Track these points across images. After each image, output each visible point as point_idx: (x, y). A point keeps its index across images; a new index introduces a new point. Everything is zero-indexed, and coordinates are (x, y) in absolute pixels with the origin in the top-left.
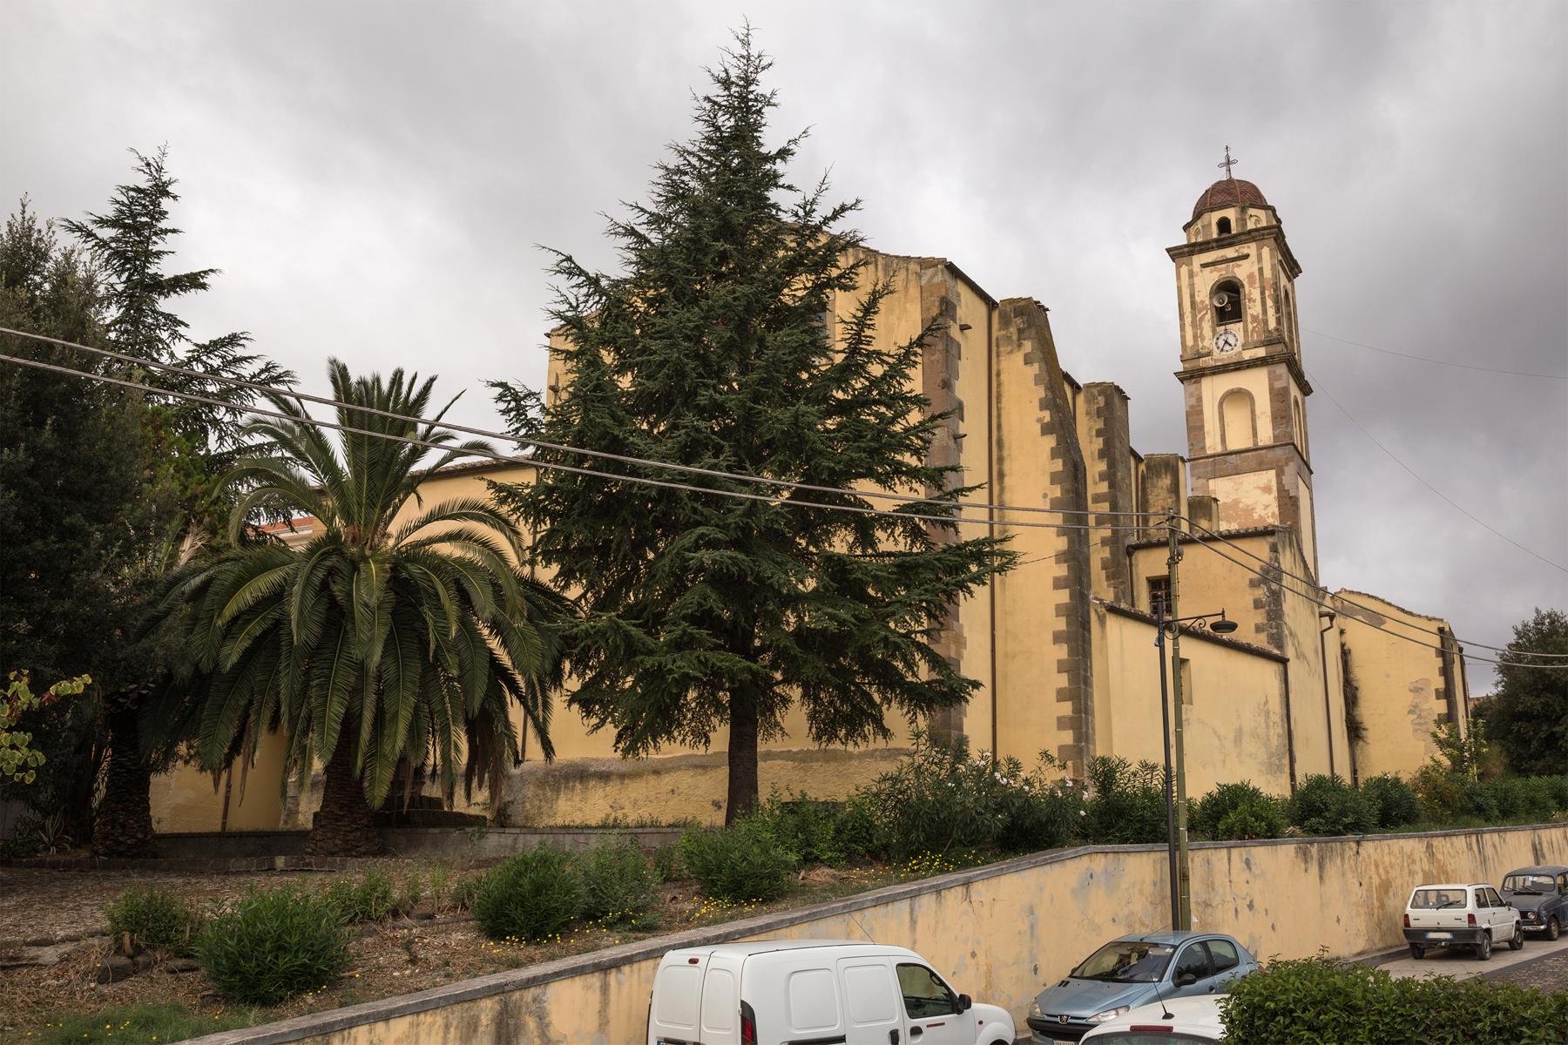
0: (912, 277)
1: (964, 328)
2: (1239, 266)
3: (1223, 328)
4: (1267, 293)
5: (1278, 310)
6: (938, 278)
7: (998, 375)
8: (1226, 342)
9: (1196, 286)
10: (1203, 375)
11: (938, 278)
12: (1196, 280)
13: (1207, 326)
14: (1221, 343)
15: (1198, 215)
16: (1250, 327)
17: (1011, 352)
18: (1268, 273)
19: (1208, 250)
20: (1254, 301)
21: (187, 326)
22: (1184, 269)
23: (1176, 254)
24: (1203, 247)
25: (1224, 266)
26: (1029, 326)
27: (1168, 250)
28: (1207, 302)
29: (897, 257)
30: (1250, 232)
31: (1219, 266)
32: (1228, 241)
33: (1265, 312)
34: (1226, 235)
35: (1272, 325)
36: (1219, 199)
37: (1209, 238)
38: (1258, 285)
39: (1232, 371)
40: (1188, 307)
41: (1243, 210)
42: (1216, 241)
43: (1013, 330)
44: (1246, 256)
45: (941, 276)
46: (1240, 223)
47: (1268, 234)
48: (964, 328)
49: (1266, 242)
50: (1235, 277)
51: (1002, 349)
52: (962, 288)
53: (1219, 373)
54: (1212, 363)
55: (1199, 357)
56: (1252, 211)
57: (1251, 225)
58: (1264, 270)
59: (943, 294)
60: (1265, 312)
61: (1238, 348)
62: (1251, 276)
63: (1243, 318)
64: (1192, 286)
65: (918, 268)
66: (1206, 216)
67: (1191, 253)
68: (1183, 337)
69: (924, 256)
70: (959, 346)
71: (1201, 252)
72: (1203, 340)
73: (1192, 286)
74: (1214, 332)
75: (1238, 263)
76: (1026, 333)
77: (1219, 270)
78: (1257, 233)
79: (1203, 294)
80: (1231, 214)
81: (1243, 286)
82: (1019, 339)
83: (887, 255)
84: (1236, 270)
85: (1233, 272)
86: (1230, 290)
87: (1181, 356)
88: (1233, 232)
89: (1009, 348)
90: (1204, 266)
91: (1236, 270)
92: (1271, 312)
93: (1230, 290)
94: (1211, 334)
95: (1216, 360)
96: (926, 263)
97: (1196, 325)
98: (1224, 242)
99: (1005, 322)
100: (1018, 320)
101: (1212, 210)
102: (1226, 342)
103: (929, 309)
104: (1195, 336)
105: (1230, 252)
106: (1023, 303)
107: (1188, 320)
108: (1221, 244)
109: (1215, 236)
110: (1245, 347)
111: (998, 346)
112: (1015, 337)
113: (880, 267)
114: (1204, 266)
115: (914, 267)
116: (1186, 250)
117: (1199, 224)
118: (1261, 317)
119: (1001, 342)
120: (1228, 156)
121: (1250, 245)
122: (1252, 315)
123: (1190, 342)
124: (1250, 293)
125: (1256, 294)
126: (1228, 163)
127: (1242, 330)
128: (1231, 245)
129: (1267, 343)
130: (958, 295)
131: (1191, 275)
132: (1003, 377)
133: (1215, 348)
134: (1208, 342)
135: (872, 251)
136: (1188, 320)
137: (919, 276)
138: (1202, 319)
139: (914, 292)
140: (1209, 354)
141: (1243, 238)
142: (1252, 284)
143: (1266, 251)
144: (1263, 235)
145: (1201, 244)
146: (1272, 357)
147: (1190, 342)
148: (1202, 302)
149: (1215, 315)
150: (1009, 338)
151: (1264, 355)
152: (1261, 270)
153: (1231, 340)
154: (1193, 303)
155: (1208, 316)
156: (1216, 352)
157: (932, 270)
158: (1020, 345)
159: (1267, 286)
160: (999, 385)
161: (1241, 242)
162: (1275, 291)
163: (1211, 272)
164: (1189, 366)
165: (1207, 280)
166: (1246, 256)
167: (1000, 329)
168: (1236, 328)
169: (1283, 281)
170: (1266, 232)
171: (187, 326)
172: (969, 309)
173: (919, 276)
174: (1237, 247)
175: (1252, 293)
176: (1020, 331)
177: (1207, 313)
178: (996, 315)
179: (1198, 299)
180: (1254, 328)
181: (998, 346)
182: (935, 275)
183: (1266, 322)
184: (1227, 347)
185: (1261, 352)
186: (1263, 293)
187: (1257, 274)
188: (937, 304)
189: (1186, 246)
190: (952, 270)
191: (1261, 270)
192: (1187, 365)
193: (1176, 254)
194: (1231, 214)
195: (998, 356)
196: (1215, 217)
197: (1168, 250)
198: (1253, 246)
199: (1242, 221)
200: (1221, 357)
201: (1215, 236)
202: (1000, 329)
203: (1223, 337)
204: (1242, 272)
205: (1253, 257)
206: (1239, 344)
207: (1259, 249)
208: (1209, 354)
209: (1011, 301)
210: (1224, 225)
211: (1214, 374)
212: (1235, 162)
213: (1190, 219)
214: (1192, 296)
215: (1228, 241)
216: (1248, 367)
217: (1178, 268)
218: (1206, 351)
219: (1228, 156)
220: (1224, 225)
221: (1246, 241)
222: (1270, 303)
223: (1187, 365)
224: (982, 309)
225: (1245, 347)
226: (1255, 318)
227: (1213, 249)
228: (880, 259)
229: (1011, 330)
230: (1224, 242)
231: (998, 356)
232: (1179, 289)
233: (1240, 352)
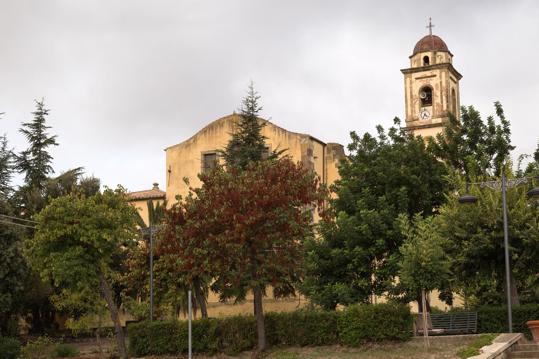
0: (298, 141)
1: (315, 158)
2: (432, 80)
3: (424, 108)
4: (443, 93)
5: (447, 102)
6: (307, 142)
7: (326, 170)
8: (425, 115)
9: (413, 88)
10: (415, 129)
11: (307, 142)
12: (413, 85)
13: (417, 106)
14: (423, 115)
15: (415, 54)
16: (435, 108)
17: (331, 162)
18: (444, 84)
19: (419, 71)
20: (438, 97)
21: (52, 158)
22: (408, 79)
23: (405, 72)
24: (416, 70)
25: (425, 79)
26: (337, 154)
27: (402, 70)
28: (418, 95)
29: (293, 133)
30: (437, 65)
31: (423, 79)
32: (427, 68)
33: (442, 102)
34: (427, 65)
35: (445, 108)
36: (425, 47)
37: (419, 66)
38: (439, 89)
39: (427, 128)
40: (409, 98)
41: (435, 53)
42: (422, 68)
43: (332, 155)
44: (435, 76)
45: (308, 141)
46: (433, 59)
47: (445, 66)
48: (315, 158)
49: (444, 70)
50: (430, 85)
51: (328, 161)
52: (315, 143)
53: (421, 128)
54: (419, 124)
55: (413, 121)
56: (439, 53)
57: (438, 62)
58: (443, 83)
59: (309, 148)
60: (442, 102)
61: (430, 118)
62: (436, 85)
63: (433, 104)
64: (411, 88)
65: (300, 138)
66: (418, 55)
67: (411, 72)
68: (407, 111)
69: (302, 133)
70: (313, 164)
71: (416, 72)
72: (415, 113)
73: (411, 88)
74: (420, 110)
75: (432, 78)
76: (336, 156)
77: (423, 81)
78: (440, 66)
79: (416, 92)
80: (429, 54)
81: (433, 89)
82: (334, 158)
83: (289, 132)
84: (431, 82)
85: (429, 82)
86: (427, 90)
87: (406, 120)
88: (430, 64)
89: (330, 161)
90: (417, 79)
91: (431, 82)
92: (445, 102)
93: (427, 90)
94: (419, 110)
95: (420, 123)
96: (303, 136)
97: (412, 106)
98: (425, 69)
99: (329, 152)
100: (333, 151)
101: (421, 52)
102: (425, 115)
103: (304, 153)
104: (412, 111)
105: (428, 73)
106: (335, 145)
107: (409, 103)
108: (424, 69)
109: (422, 65)
110: (433, 117)
111: (326, 160)
112: (332, 157)
113: (287, 136)
114: (417, 79)
115: (298, 137)
116: (409, 71)
117: (416, 58)
118: (440, 104)
119: (327, 159)
120: (430, 23)
121: (437, 70)
122: (436, 103)
123: (409, 114)
124: (436, 93)
125: (438, 93)
126: (431, 26)
127: (432, 110)
128: (429, 70)
129: (443, 116)
130: (313, 146)
131: (411, 82)
132: (328, 171)
133: (420, 117)
134: (417, 114)
135: (284, 130)
136: (409, 103)
137: (300, 141)
138: (415, 103)
139: (299, 146)
140: (417, 120)
141: (434, 67)
142: (437, 89)
143: (443, 74)
144: (442, 66)
145: (415, 69)
146: (444, 123)
147: (409, 114)
148: (415, 95)
149: (420, 102)
150: (330, 157)
151: (441, 122)
152: (441, 82)
153: (427, 114)
154: (411, 96)
155: (418, 102)
156: (420, 119)
157: (304, 139)
158: (334, 160)
159: (443, 90)
160: (327, 174)
161: (433, 69)
162: (447, 92)
163: (420, 82)
164: (410, 124)
165: (418, 85)
166: (435, 76)
167: (327, 154)
168: (429, 108)
169: (452, 85)
170: (443, 65)
171: (52, 158)
172: (317, 150)
173: (300, 141)
174: (431, 71)
175: (437, 93)
176: (334, 155)
177: (417, 101)
178: (326, 148)
179: (413, 94)
180: (437, 109)
181: (326, 160)
182: (305, 141)
183: (442, 107)
184: (425, 117)
185: (440, 120)
186: (441, 93)
187: (439, 84)
188: (306, 151)
189: (409, 69)
190: (312, 139)
191: (441, 82)
192: (408, 124)
193: (405, 72)
194: (429, 54)
195: (326, 163)
196: (423, 55)
197: (402, 70)
198: (438, 71)
199: (434, 59)
200: (422, 121)
201: (422, 65)
202: (327, 154)
203: (424, 112)
204: (433, 83)
205: (438, 76)
206: (430, 116)
207: (441, 73)
208: (417, 120)
209: (331, 144)
210: (426, 59)
211: (419, 129)
212: (434, 26)
213: (412, 54)
214: (411, 92)
215: (427, 68)
216: (434, 127)
217: (405, 78)
218: (416, 118)
219: (430, 23)
220: (426, 59)
221: (435, 69)
222: (444, 98)
223: (408, 124)
224: (321, 147)
225: (433, 117)
226: (438, 104)
227: (420, 71)
228: (287, 133)
229: (331, 154)
230: (425, 69)
231: (326, 163)
232: (406, 88)
233: (431, 120)
